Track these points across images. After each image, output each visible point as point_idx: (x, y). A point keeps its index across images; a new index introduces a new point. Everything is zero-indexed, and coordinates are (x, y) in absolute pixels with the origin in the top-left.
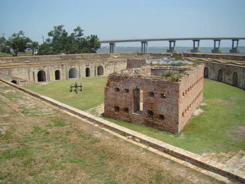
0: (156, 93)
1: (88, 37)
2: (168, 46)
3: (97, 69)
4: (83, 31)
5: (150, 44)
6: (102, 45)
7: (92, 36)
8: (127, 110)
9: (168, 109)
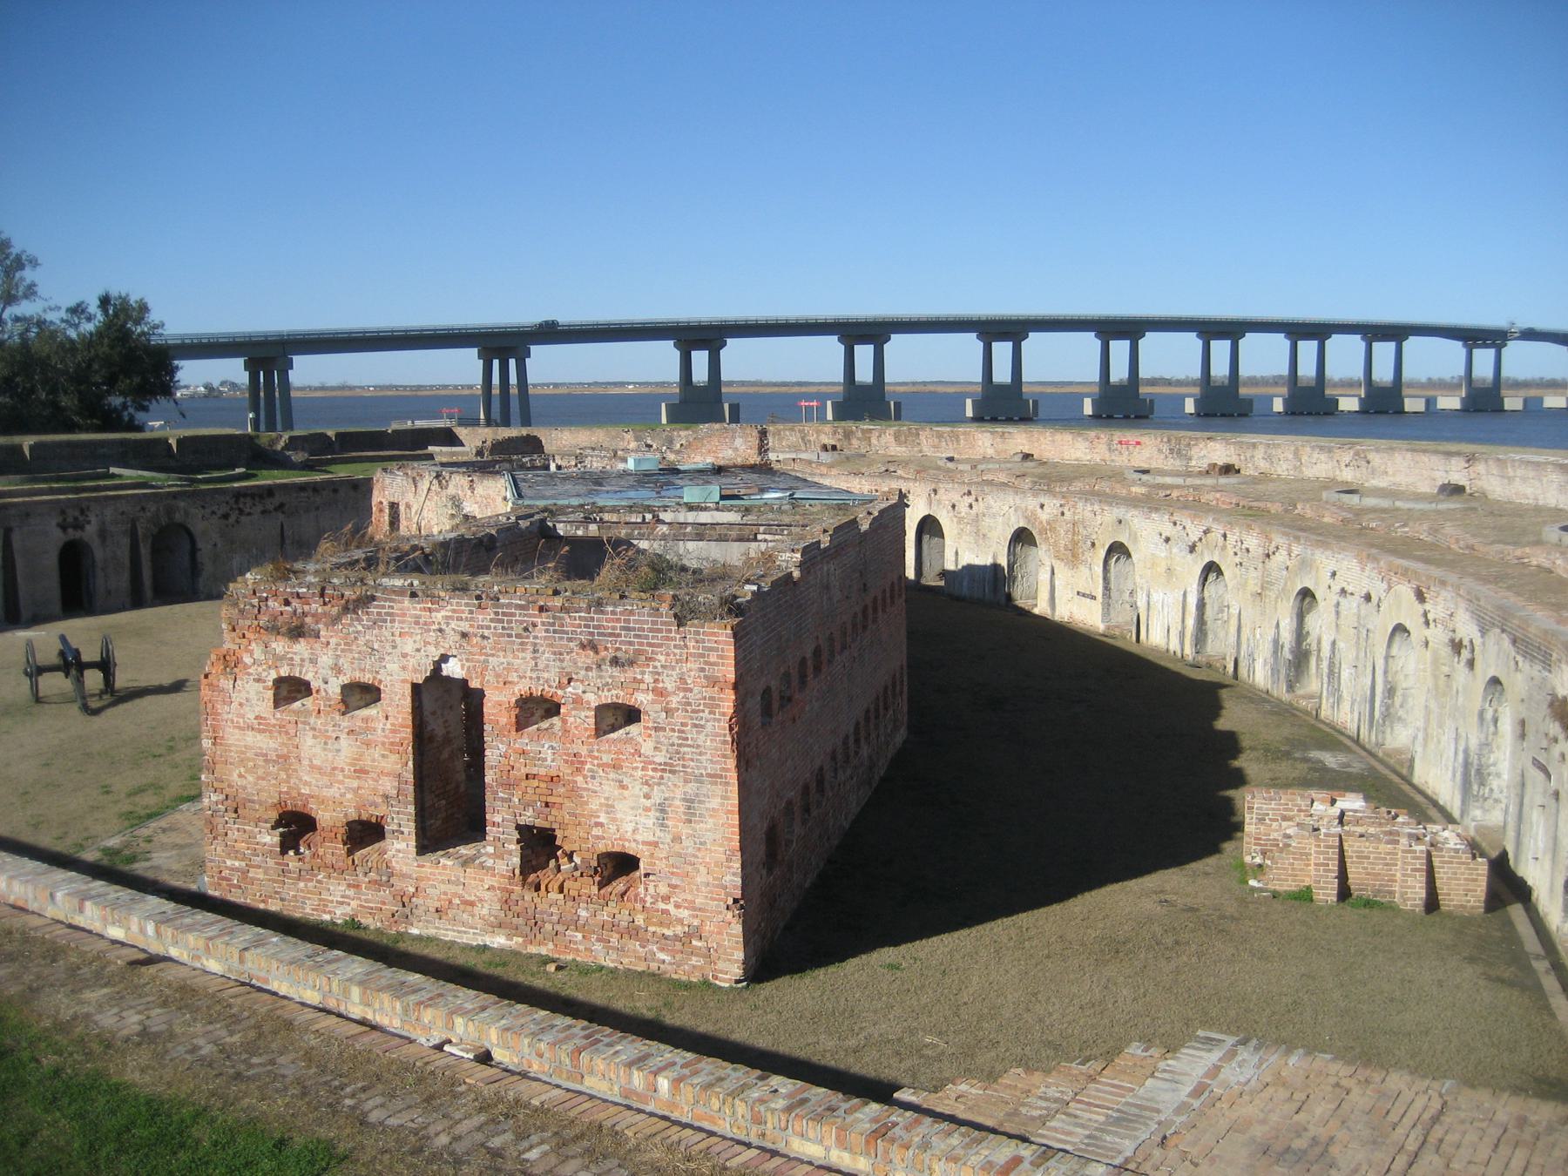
0: (578, 701)
1: (78, 310)
2: (674, 375)
3: (145, 551)
4: (34, 263)
5: (307, 372)
6: (193, 375)
7: (105, 301)
8: (364, 833)
9: (662, 809)
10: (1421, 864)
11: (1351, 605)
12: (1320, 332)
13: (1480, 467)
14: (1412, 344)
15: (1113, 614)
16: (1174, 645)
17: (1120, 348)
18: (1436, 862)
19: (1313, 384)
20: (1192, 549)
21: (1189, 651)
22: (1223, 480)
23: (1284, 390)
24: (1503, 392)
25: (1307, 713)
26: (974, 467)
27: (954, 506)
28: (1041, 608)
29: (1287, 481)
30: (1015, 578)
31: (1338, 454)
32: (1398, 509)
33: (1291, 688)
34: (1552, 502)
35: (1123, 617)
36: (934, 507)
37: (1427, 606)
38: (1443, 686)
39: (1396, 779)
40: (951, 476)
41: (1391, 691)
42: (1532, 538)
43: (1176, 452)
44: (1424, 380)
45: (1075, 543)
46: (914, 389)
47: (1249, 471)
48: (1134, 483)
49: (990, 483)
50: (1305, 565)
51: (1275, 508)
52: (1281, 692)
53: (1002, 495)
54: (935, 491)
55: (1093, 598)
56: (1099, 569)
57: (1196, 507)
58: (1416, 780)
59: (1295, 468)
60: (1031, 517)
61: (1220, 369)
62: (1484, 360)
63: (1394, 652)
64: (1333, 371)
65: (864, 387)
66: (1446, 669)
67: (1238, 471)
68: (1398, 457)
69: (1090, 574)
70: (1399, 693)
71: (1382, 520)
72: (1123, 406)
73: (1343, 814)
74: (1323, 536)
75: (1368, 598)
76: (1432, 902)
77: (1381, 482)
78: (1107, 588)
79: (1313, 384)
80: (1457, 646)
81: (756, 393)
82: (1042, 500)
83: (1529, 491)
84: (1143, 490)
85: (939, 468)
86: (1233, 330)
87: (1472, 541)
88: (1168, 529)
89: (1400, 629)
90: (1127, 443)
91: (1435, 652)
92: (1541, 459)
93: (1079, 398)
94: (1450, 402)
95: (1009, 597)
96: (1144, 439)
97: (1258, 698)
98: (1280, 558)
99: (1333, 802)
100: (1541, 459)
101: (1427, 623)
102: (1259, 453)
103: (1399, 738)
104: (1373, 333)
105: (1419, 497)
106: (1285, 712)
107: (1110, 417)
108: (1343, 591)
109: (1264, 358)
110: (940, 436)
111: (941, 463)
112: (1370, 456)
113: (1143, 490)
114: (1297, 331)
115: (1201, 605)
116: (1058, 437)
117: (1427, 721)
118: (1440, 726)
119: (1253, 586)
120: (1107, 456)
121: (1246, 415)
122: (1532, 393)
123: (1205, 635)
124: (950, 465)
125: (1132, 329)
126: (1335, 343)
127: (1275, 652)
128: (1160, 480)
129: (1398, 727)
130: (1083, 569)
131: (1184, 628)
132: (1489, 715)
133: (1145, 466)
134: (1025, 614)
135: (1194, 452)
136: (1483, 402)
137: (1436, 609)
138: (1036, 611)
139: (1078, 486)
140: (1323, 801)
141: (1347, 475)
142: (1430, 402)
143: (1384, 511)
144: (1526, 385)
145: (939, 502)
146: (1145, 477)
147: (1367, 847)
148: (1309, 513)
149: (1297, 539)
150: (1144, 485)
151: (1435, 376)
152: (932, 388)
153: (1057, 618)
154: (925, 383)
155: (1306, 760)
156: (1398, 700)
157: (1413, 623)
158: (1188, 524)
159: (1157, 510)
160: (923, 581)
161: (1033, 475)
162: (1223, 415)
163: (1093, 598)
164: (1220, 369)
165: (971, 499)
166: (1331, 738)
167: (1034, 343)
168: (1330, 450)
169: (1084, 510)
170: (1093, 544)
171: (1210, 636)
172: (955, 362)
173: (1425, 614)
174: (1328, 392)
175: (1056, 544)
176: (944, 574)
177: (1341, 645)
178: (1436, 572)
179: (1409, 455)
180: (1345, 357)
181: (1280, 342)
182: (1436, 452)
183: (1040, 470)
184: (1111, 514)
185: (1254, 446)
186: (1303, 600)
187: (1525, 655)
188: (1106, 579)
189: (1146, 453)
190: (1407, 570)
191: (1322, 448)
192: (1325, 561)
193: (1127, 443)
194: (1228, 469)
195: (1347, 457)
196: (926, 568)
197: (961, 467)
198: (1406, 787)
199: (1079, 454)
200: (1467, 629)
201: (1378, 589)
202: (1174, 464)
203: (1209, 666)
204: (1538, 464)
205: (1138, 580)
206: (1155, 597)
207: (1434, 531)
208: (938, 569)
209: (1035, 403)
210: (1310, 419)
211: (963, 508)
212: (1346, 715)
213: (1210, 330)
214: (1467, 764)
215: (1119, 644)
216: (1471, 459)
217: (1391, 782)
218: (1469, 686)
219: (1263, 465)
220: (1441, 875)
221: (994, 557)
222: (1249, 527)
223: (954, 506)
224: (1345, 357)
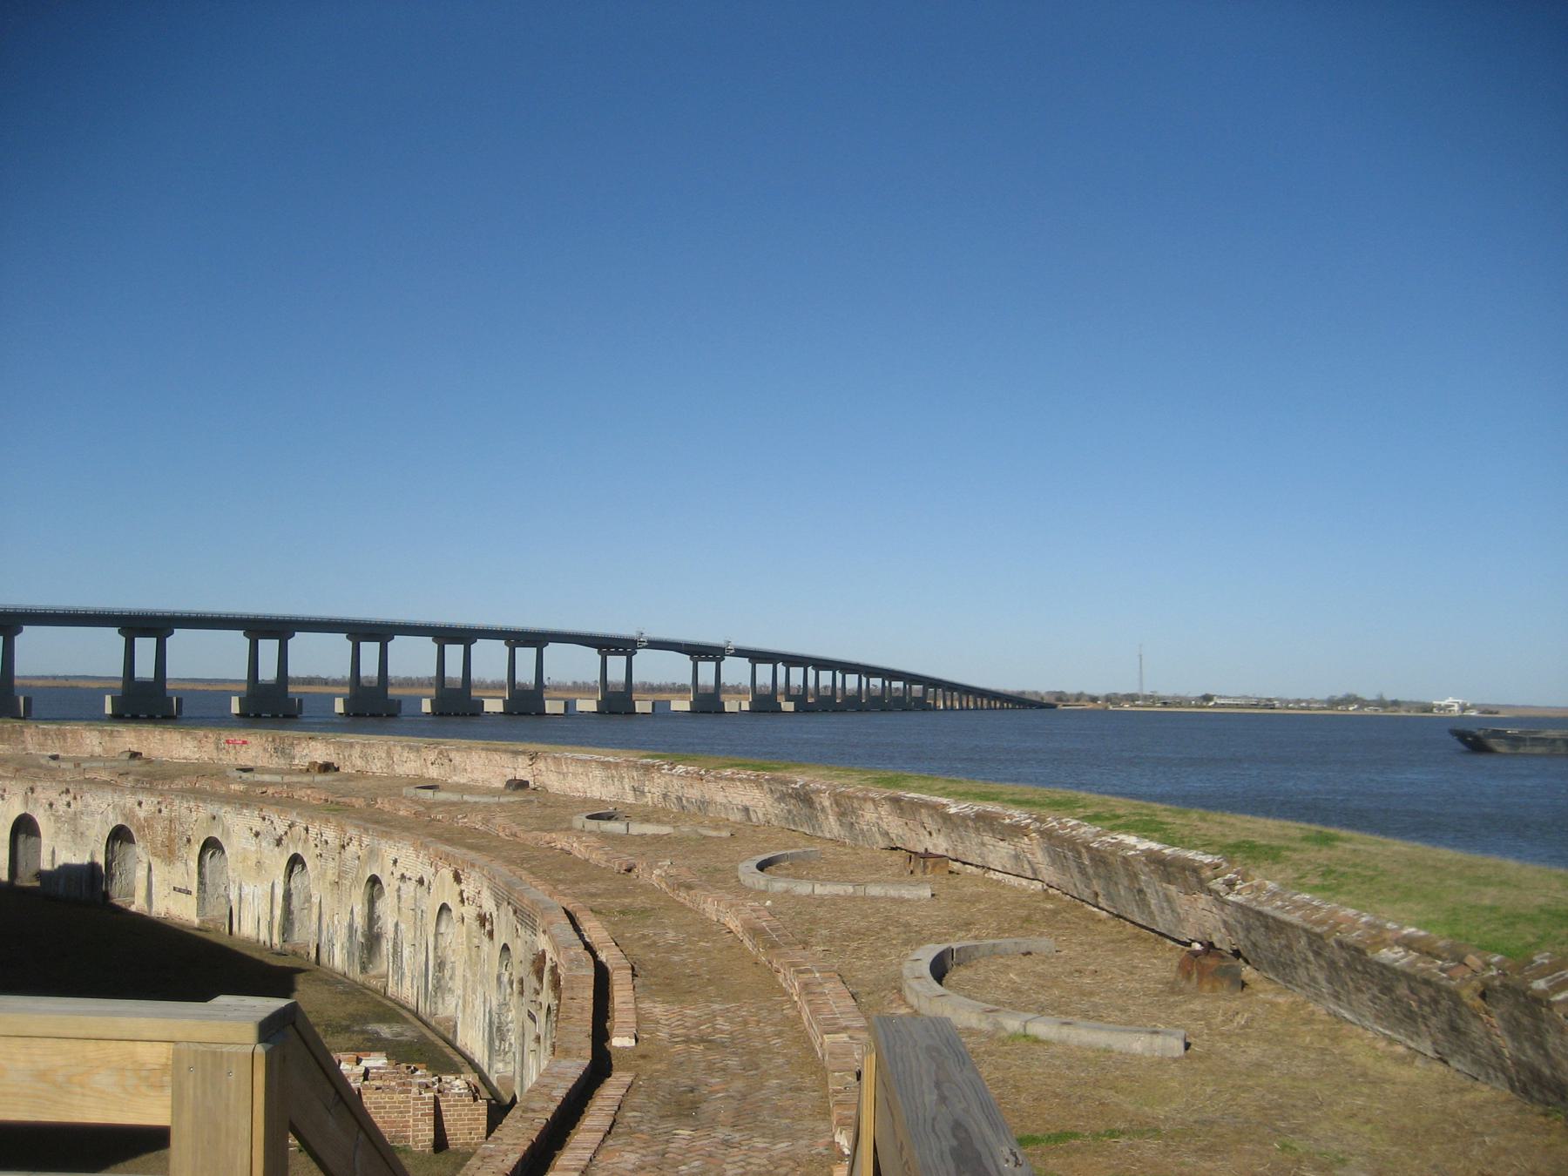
10: (429, 1109)
11: (409, 888)
12: (467, 636)
13: (541, 765)
14: (551, 649)
15: (208, 909)
16: (264, 936)
17: (268, 648)
18: (443, 1106)
19: (459, 686)
20: (279, 842)
21: (276, 940)
22: (320, 778)
23: (432, 692)
24: (635, 696)
25: (377, 992)
26: (77, 765)
27: (51, 805)
28: (138, 905)
29: (379, 778)
30: (113, 876)
31: (424, 753)
32: (466, 802)
33: (364, 969)
34: (597, 795)
35: (217, 911)
36: (31, 806)
37: (463, 886)
38: (474, 961)
39: (441, 1043)
40: (51, 774)
41: (441, 965)
42: (565, 826)
43: (281, 751)
44: (569, 684)
45: (171, 840)
46: (55, 683)
47: (346, 769)
48: (234, 781)
49: (92, 781)
50: (373, 854)
51: (359, 803)
52: (356, 974)
53: (100, 793)
54: (32, 790)
55: (189, 893)
56: (194, 865)
57: (285, 802)
58: (458, 1044)
59: (388, 766)
60: (130, 815)
61: (369, 669)
62: (707, 670)
63: (442, 929)
64: (726, 679)
65: (144, 684)
66: (476, 941)
67: (337, 769)
68: (475, 756)
69: (185, 871)
70: (448, 966)
71: (449, 812)
72: (271, 705)
73: (367, 1071)
74: (386, 825)
75: (421, 882)
76: (440, 1142)
77: (461, 779)
78: (202, 883)
79: (375, 684)
80: (482, 919)
81: (193, 691)
82: (140, 798)
83: (580, 785)
84: (242, 787)
85: (40, 767)
86: (381, 633)
87: (516, 829)
88: (257, 824)
89: (444, 908)
90: (234, 742)
91: (469, 928)
92: (587, 757)
93: (227, 695)
94: (587, 705)
95: (106, 895)
96: (249, 739)
97: (333, 980)
98: (353, 848)
99: (358, 1061)
100: (587, 757)
101: (462, 901)
102: (356, 752)
103: (448, 1007)
104: (516, 639)
105: (491, 792)
106: (355, 991)
107: (258, 716)
108: (403, 876)
109: (412, 660)
110: (45, 734)
111: (43, 761)
112: (452, 755)
113: (242, 787)
114: (444, 635)
115: (288, 896)
116: (167, 736)
117: (465, 989)
118: (474, 993)
119: (331, 876)
120: (215, 755)
121: (295, 717)
122: (664, 696)
123: (292, 924)
124: (53, 764)
125: (282, 629)
126: (480, 647)
127: (350, 937)
128: (258, 777)
129: (448, 997)
130: (180, 865)
131: (272, 918)
132: (505, 979)
133: (251, 764)
134: (122, 912)
135: (298, 751)
136: (526, 705)
137: (469, 889)
138: (133, 908)
139: (179, 784)
140: (348, 1061)
141: (433, 773)
142: (569, 705)
143: (453, 804)
144: (652, 689)
145: (36, 800)
146: (245, 775)
147: (383, 1098)
148: (387, 807)
149: (366, 830)
150: (243, 782)
151: (580, 681)
152: (74, 683)
153: (154, 914)
154: (66, 678)
155: (363, 1032)
156: (447, 973)
157: (453, 903)
158: (275, 818)
159: (247, 806)
160: (18, 883)
161: (137, 773)
162: (372, 715)
163: (189, 893)
164: (369, 669)
165: (66, 798)
166: (391, 1011)
167: (179, 639)
168: (418, 750)
169: (180, 807)
170: (189, 841)
171: (297, 925)
172: (97, 656)
173: (461, 893)
174: (474, 693)
175: (152, 842)
176: (41, 875)
177: (402, 926)
178: (472, 855)
179: (483, 754)
180: (489, 661)
181: (428, 645)
182: (506, 751)
183: (147, 768)
184: (205, 811)
185: (351, 745)
186: (373, 887)
187: (522, 922)
188: (201, 874)
189: (252, 752)
190: (448, 855)
191: (411, 748)
192: (389, 850)
193: (234, 742)
194: (327, 768)
195: (432, 756)
196: (21, 869)
197: (63, 765)
198: (449, 1050)
199: (187, 753)
200: (489, 906)
201: (428, 872)
202: (278, 762)
203: (295, 953)
204: (585, 761)
205: (230, 873)
206: (246, 890)
207: (486, 821)
208: (33, 870)
209: (179, 701)
210: (458, 720)
211: (60, 806)
212: (407, 991)
213: (359, 632)
214: (491, 1023)
215: (211, 937)
216: (534, 757)
217: (436, 1046)
218: (490, 950)
219: (359, 763)
220: (448, 1118)
221: (92, 855)
222: (327, 821)
223: (51, 805)
224: (489, 661)
